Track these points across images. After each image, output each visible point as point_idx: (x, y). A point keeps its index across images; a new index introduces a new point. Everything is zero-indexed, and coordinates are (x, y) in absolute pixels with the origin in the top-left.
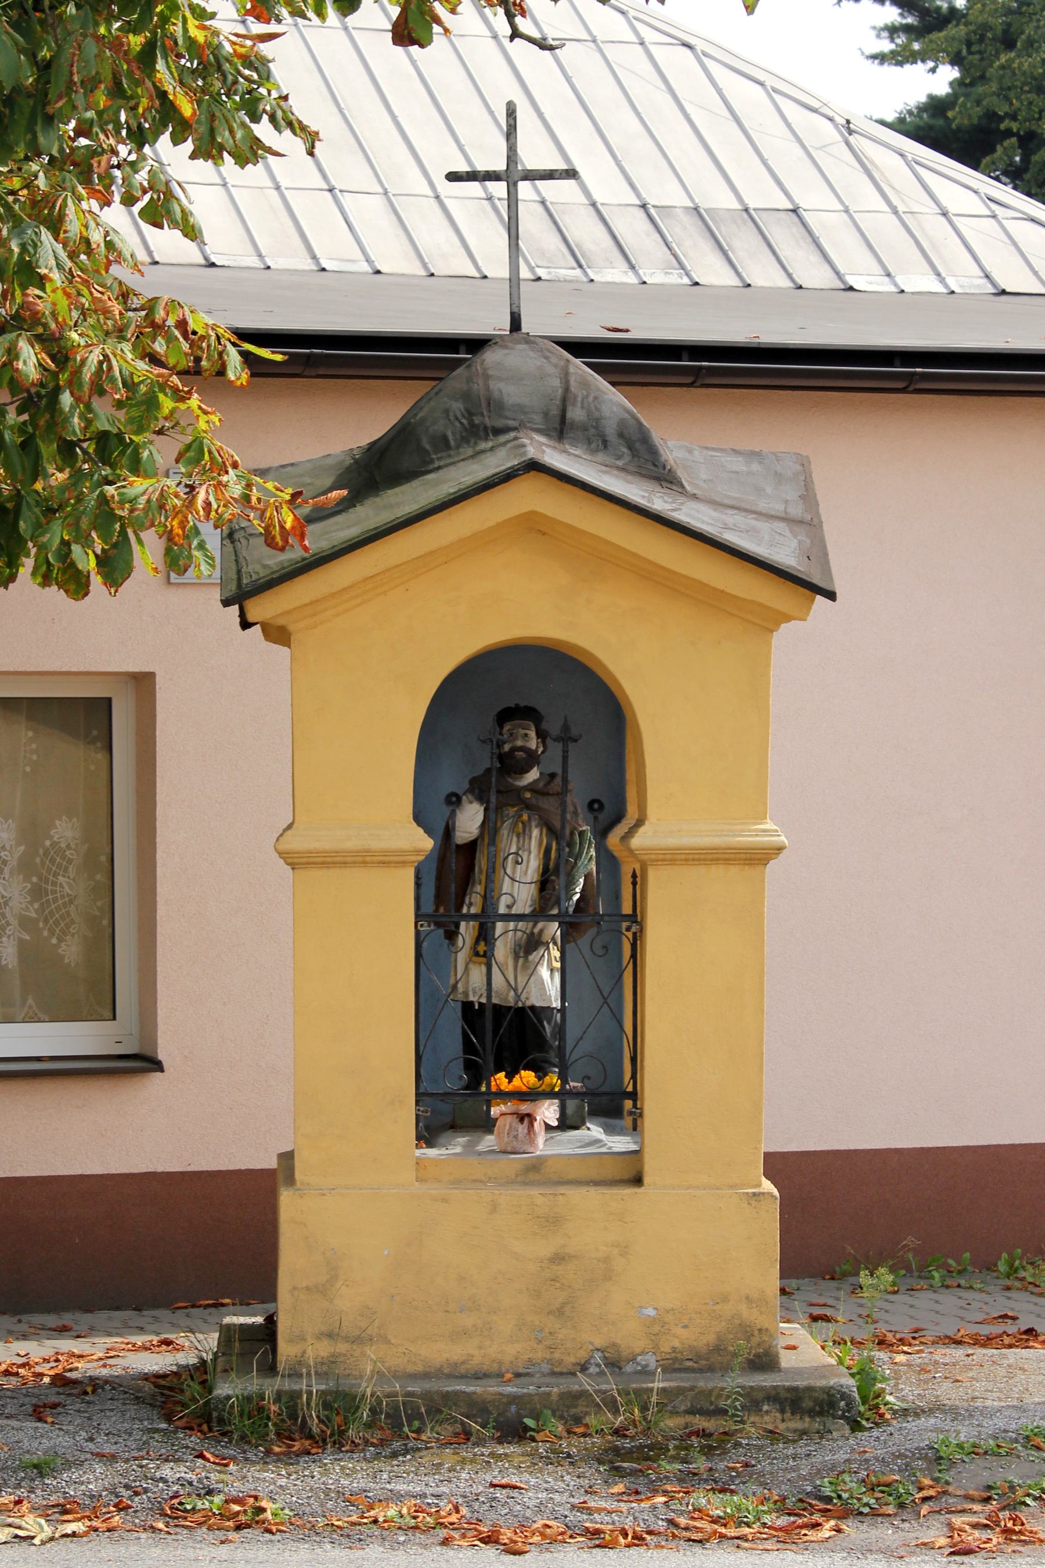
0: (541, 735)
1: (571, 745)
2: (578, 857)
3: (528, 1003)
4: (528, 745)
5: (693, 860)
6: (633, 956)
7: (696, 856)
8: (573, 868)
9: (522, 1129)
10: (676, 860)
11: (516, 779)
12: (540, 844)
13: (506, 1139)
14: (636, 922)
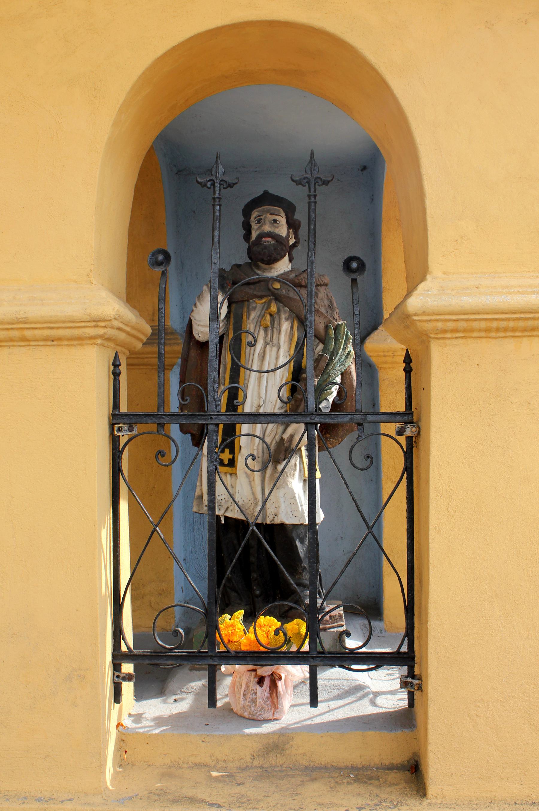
0: (293, 225)
1: (321, 189)
2: (333, 354)
3: (277, 521)
4: (277, 231)
5: (497, 330)
6: (409, 470)
7: (503, 324)
8: (328, 365)
9: (262, 692)
10: (472, 330)
11: (264, 270)
12: (291, 340)
13: (242, 702)
14: (411, 422)
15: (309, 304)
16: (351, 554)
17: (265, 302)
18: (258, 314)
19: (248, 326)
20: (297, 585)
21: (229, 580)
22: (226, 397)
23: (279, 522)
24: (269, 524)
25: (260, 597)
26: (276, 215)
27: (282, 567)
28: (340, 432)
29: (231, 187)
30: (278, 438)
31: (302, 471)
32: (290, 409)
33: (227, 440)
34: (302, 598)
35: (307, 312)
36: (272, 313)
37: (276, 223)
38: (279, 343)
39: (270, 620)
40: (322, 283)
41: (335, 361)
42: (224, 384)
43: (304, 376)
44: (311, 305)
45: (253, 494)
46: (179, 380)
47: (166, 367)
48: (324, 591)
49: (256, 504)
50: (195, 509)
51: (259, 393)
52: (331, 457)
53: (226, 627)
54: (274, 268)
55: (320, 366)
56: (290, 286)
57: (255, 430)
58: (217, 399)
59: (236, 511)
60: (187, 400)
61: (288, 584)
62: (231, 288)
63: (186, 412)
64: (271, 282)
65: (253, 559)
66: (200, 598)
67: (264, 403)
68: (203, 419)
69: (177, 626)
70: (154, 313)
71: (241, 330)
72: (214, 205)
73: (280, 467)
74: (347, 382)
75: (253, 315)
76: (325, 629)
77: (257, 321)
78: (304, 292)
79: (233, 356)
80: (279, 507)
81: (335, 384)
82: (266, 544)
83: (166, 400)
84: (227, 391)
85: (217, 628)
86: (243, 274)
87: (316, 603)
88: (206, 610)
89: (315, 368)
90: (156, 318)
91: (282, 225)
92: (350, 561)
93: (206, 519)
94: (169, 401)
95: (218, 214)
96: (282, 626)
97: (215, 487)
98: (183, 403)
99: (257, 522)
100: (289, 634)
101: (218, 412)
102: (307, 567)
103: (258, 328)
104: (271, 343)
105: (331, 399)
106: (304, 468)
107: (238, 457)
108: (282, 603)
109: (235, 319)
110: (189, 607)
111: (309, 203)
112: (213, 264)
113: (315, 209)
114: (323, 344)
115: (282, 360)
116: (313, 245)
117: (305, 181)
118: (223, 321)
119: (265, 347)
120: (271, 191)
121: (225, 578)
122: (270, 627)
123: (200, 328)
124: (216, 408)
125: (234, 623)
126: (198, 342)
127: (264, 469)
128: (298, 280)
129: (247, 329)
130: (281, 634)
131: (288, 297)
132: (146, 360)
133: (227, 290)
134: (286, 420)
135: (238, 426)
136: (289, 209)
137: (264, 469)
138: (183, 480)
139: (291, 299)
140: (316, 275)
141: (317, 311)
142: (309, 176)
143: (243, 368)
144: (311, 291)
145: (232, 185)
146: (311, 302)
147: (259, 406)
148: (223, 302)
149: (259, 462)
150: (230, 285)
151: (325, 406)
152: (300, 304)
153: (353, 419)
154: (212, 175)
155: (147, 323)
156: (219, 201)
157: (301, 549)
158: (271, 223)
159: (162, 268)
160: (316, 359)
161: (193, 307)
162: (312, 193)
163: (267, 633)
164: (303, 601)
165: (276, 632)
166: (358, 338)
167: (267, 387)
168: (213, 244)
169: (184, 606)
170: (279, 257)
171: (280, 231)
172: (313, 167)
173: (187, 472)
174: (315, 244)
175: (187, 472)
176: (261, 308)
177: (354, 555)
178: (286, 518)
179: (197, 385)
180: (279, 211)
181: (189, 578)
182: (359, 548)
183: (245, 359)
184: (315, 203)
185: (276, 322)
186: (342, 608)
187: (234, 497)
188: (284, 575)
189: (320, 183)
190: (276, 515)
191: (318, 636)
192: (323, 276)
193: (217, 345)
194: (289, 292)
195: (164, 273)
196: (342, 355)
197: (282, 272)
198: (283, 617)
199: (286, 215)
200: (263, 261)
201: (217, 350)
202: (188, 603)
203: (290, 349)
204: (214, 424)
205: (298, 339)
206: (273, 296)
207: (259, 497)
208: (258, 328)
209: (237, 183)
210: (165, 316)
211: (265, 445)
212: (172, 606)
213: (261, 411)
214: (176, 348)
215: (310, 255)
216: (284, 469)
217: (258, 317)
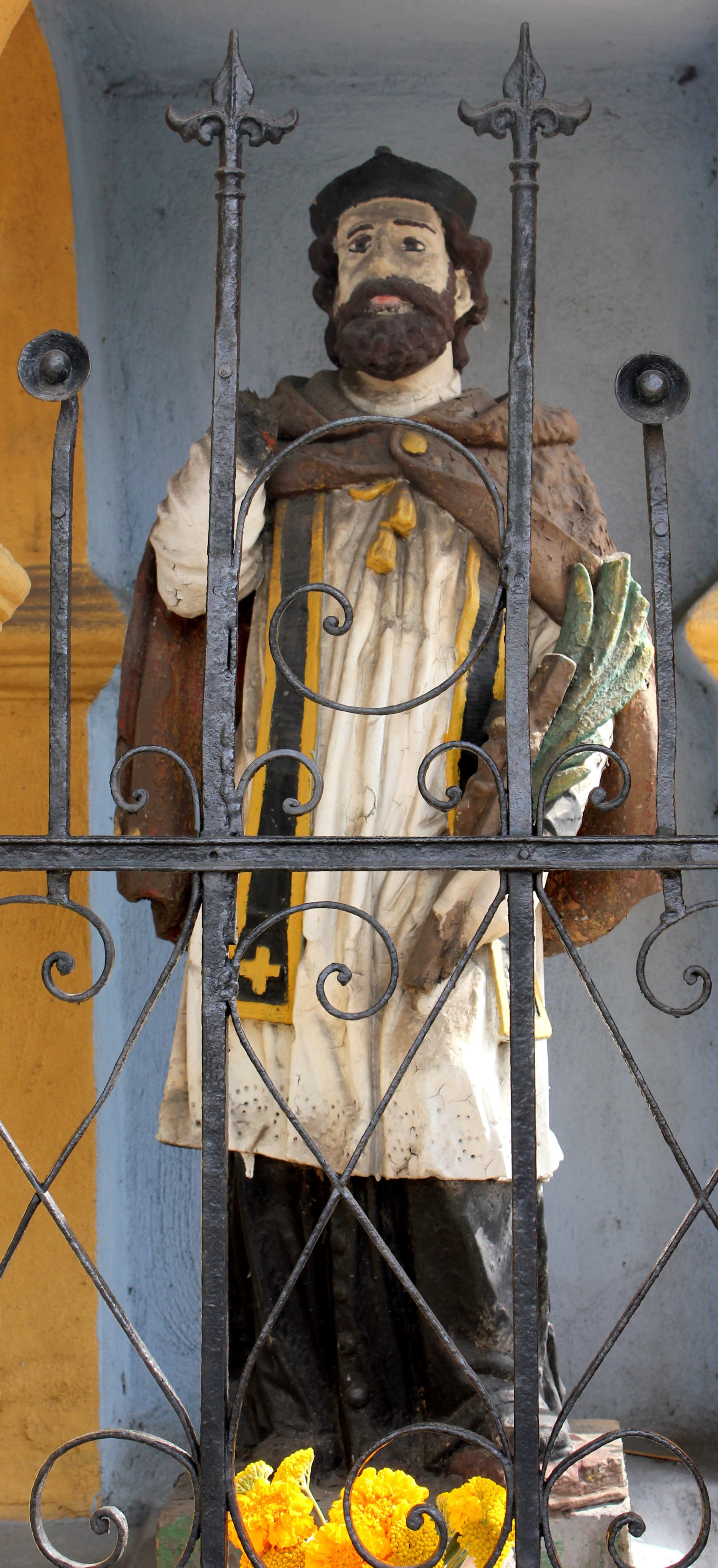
0: (465, 255)
2: (590, 654)
3: (418, 1170)
4: (417, 275)
8: (573, 688)
11: (378, 396)
12: (460, 611)
15: (513, 503)
16: (646, 1274)
17: (380, 494)
18: (359, 532)
19: (329, 567)
20: (478, 1371)
21: (268, 1353)
22: (261, 788)
23: (422, 1174)
24: (392, 1180)
25: (364, 1406)
26: (415, 224)
27: (430, 1314)
28: (612, 896)
29: (276, 141)
30: (419, 913)
31: (494, 1016)
32: (456, 824)
33: (261, 919)
34: (495, 1413)
35: (508, 529)
36: (402, 530)
37: (415, 249)
38: (423, 623)
39: (394, 1482)
40: (556, 437)
41: (595, 678)
42: (254, 749)
43: (499, 722)
44: (519, 506)
45: (344, 1085)
46: (115, 735)
47: (73, 695)
48: (563, 1389)
49: (353, 1119)
50: (164, 1133)
51: (361, 776)
52: (582, 973)
53: (260, 1503)
54: (408, 389)
55: (549, 691)
56: (457, 449)
57: (349, 891)
58: (232, 796)
59: (290, 1139)
60: (138, 799)
61: (452, 1368)
62: (275, 453)
63: (137, 833)
64: (397, 434)
65: (341, 1289)
66: (178, 1410)
67: (378, 805)
68: (188, 857)
69: (107, 1501)
70: (37, 528)
71: (305, 581)
72: (221, 198)
73: (426, 1005)
74: (631, 739)
75: (344, 534)
76: (565, 1511)
77: (356, 554)
78: (498, 462)
79: (282, 662)
80: (423, 1127)
81: (592, 748)
82: (380, 1242)
83: (74, 797)
84: (263, 770)
85: (229, 1505)
86: (312, 410)
87: (535, 1427)
88: (197, 1448)
89: (533, 700)
90: (45, 543)
91: (433, 256)
92: (640, 1296)
93: (198, 1164)
94: (84, 801)
95: (233, 223)
96: (431, 1499)
97: (224, 1066)
98: (127, 806)
99: (356, 1172)
100: (455, 1525)
101: (234, 834)
102: (509, 1314)
103: (357, 574)
104: (398, 622)
105: (582, 791)
106: (499, 1007)
107: (296, 971)
108: (431, 1426)
109: (289, 545)
110: (143, 1441)
111: (516, 190)
112: (218, 381)
113: (534, 210)
114: (560, 623)
115: (435, 673)
116: (526, 321)
117: (503, 121)
118: (251, 552)
119: (381, 634)
120: (398, 151)
121: (255, 1350)
122: (395, 1502)
123: (180, 576)
124: (229, 823)
125: (283, 1489)
126: (175, 620)
127: (376, 1009)
128: (483, 425)
129: (326, 579)
130: (429, 1524)
131: (451, 479)
132: (13, 672)
133: (264, 457)
134: (445, 858)
135: (296, 877)
136: (455, 206)
137: (376, 1009)
138: (128, 1042)
139: (458, 484)
140: (537, 411)
141: (542, 523)
142: (514, 105)
143: (313, 699)
144: (521, 464)
145: (277, 134)
146: (520, 496)
147: (362, 816)
148: (249, 498)
149: (360, 988)
150: (273, 441)
151: (565, 815)
152: (488, 500)
153: (651, 856)
154: (214, 102)
155: (17, 559)
156: (238, 184)
157: (492, 1257)
158: (397, 250)
159: (62, 393)
160: (538, 671)
161: (159, 511)
162: (525, 159)
163: (384, 1522)
164: (496, 1422)
165: (414, 1520)
166: (666, 607)
167: (385, 756)
168: (218, 319)
169: (127, 1437)
170: (422, 354)
171: (427, 274)
172: (527, 78)
173: (140, 1020)
174: (531, 317)
175: (140, 1020)
176: (367, 514)
177: (653, 1278)
178: (445, 1159)
179: (171, 753)
180: (423, 213)
181: (144, 1350)
182: (668, 1256)
183: (320, 671)
184: (535, 189)
185: (413, 558)
186: (619, 1442)
187: (282, 1095)
188: (438, 1338)
189: (550, 128)
190: (413, 1152)
191: (543, 1531)
192: (559, 415)
193: (230, 630)
194: (453, 465)
195: (67, 408)
196: (617, 657)
197: (432, 400)
198: (437, 1472)
199: (446, 225)
200: (373, 369)
201: (230, 646)
202: (141, 1427)
203: (456, 639)
204: (223, 872)
205: (482, 608)
206: (406, 476)
207: (362, 1094)
208: (357, 574)
209: (291, 128)
210: (70, 542)
211: (378, 936)
212: (92, 1438)
213: (368, 831)
214: (106, 636)
215: (516, 353)
216: (437, 1010)
217: (360, 541)
